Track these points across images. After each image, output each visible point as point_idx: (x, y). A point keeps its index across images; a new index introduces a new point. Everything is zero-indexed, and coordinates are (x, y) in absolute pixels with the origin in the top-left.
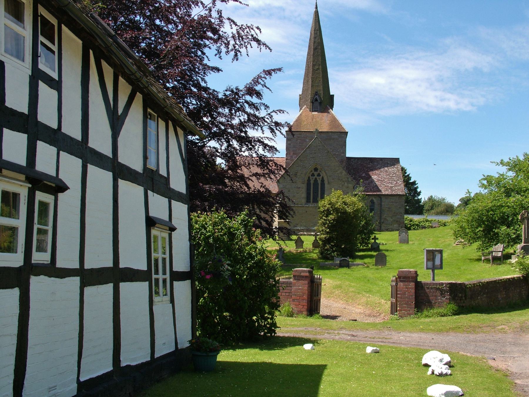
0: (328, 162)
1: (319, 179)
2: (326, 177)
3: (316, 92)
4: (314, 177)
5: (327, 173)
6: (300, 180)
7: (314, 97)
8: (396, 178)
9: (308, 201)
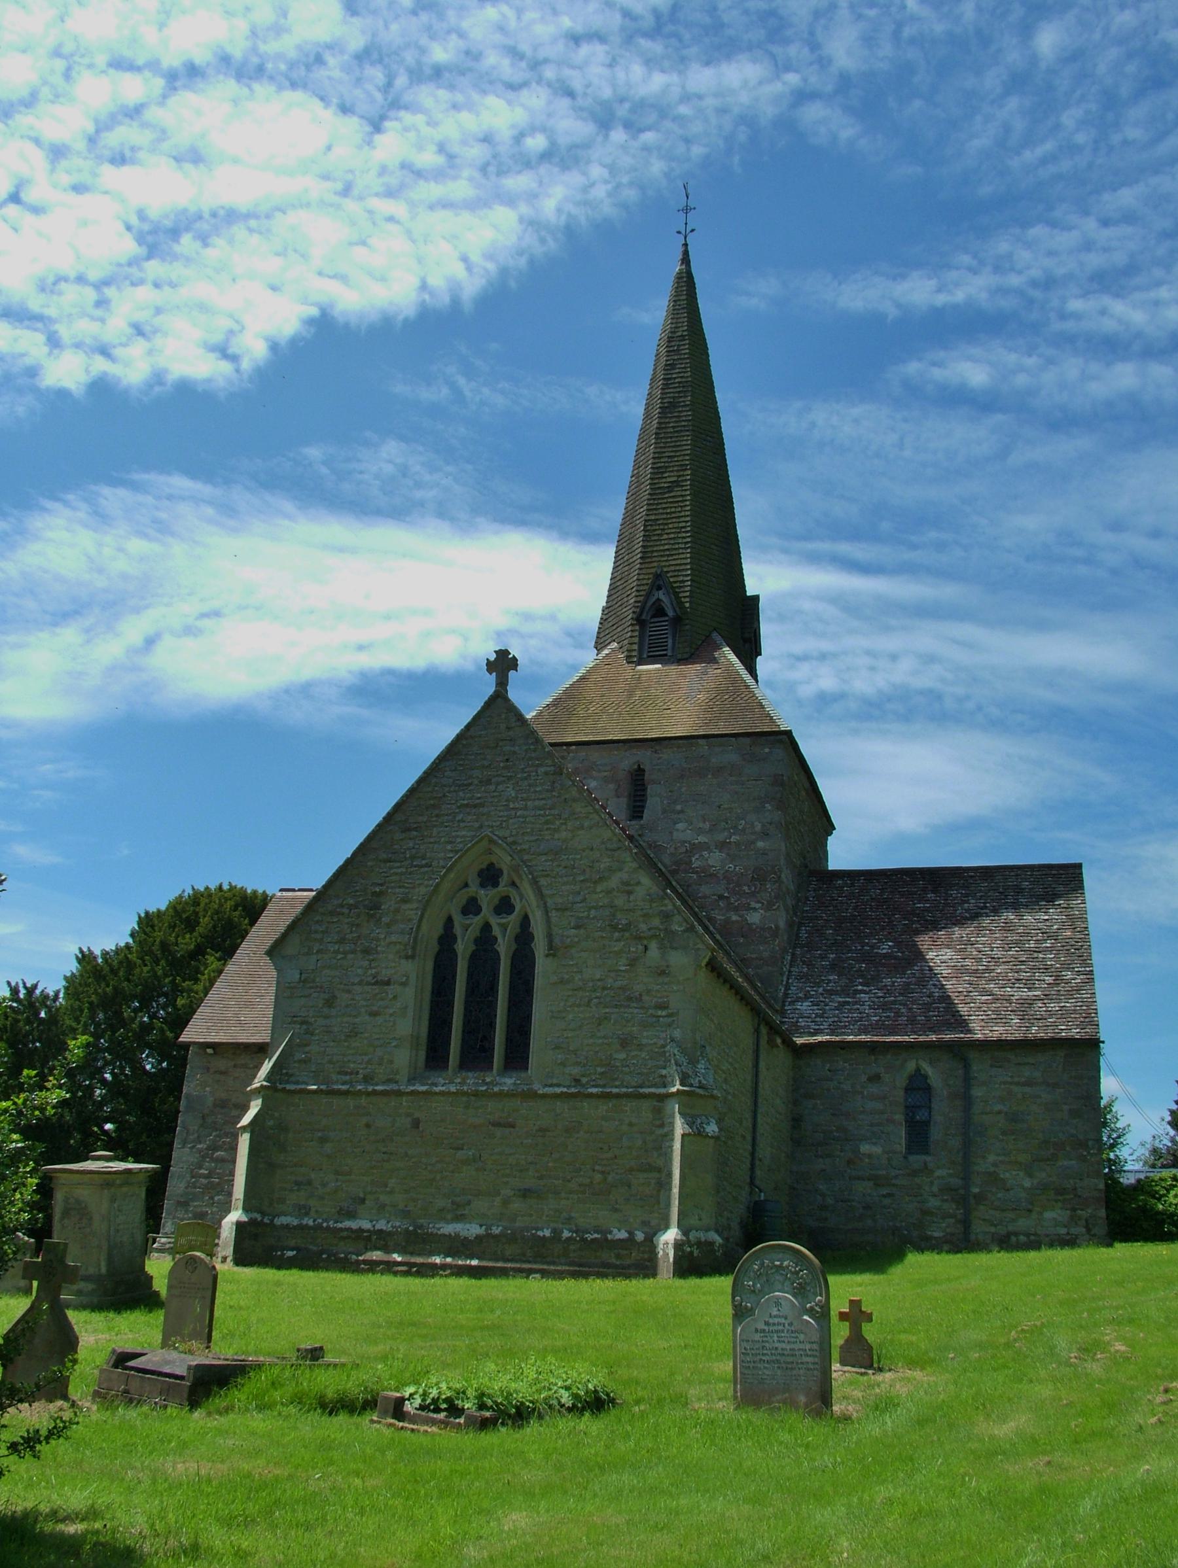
0: (557, 830)
1: (504, 927)
3: (658, 576)
4: (476, 921)
5: (546, 892)
6: (393, 938)
7: (648, 595)
8: (1056, 958)
9: (436, 1056)
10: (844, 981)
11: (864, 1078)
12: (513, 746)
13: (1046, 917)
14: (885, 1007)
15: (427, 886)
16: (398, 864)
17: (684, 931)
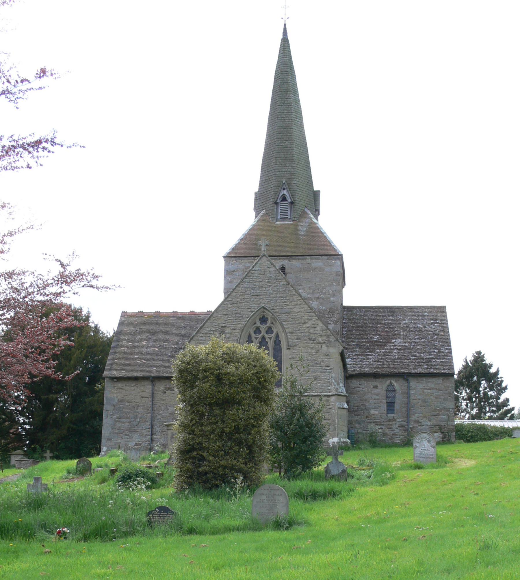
2: (283, 334)
4: (260, 336)
10: (362, 350)
11: (372, 387)
12: (271, 274)
13: (434, 327)
14: (378, 361)
15: (242, 324)
16: (231, 316)
17: (334, 341)
